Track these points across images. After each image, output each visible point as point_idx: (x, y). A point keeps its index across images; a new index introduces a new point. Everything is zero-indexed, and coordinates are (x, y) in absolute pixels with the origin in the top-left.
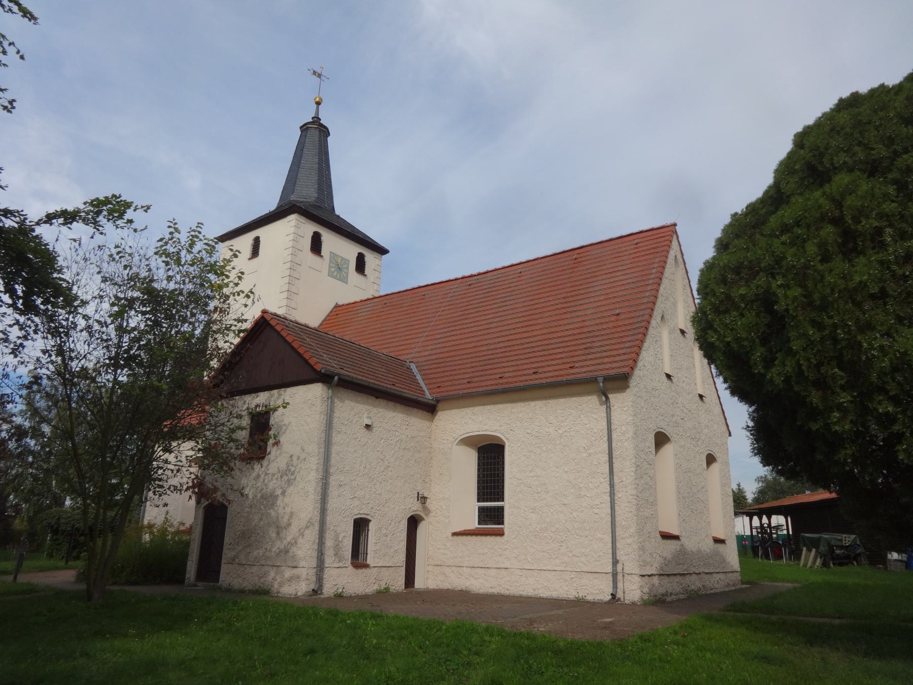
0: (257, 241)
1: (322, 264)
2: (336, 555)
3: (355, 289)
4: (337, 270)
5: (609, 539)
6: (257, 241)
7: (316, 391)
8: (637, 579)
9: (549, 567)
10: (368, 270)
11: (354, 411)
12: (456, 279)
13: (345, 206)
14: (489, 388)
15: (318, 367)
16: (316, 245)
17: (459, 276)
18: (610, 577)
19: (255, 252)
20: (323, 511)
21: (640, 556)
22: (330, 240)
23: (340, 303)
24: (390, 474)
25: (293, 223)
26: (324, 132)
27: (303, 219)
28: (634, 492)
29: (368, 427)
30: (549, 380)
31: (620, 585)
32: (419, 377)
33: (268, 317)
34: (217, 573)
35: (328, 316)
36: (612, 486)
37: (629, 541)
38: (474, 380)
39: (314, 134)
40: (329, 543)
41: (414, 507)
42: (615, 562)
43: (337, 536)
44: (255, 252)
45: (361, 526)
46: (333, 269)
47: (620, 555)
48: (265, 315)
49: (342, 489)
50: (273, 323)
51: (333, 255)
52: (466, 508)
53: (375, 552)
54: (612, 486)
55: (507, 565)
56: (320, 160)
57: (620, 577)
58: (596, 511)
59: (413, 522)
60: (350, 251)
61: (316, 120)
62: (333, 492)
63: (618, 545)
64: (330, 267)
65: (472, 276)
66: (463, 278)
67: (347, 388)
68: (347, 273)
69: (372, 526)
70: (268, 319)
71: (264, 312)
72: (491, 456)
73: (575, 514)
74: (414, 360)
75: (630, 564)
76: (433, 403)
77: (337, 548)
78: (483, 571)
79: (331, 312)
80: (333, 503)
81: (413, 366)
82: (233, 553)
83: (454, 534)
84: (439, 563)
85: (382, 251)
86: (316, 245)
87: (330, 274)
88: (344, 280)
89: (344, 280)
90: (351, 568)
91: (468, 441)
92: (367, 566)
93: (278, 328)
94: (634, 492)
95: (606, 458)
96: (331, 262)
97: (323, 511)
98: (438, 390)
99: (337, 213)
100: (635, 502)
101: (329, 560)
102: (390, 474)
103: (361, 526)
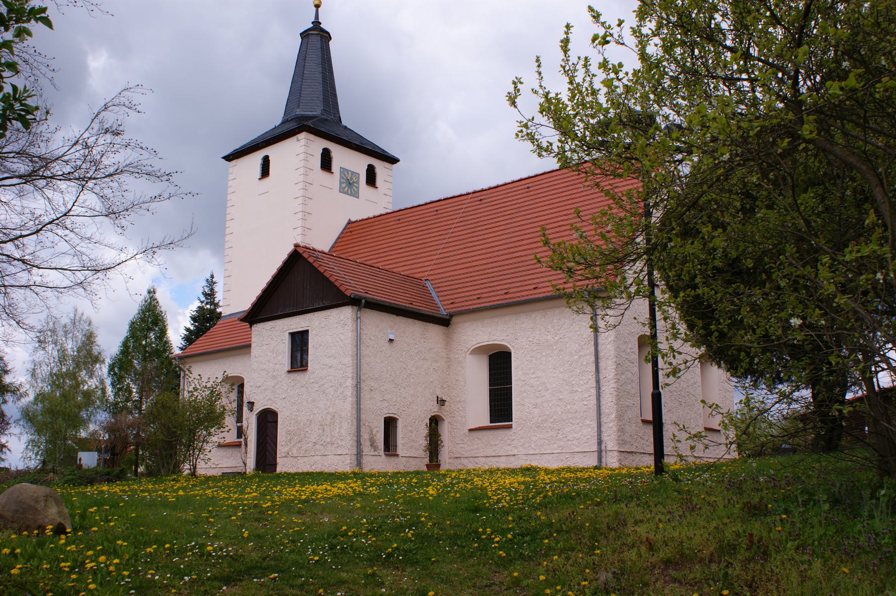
0: (266, 162)
1: (333, 180)
2: (372, 445)
3: (371, 204)
4: (349, 185)
5: (594, 425)
6: (266, 162)
7: (346, 313)
8: (616, 454)
9: (548, 451)
10: (379, 181)
11: (379, 326)
12: (468, 194)
13: (351, 116)
14: (495, 303)
15: (348, 293)
16: (326, 163)
17: (471, 191)
18: (596, 454)
19: (265, 171)
20: (359, 410)
21: (619, 436)
22: (342, 157)
23: (353, 220)
24: (412, 381)
25: (303, 142)
26: (325, 37)
27: (312, 137)
28: (614, 385)
29: (391, 340)
30: (544, 295)
31: (604, 460)
32: (434, 294)
33: (300, 250)
34: (275, 465)
35: (342, 233)
36: (598, 381)
37: (610, 425)
38: (483, 296)
39: (315, 41)
40: (365, 436)
41: (434, 410)
42: (600, 443)
43: (371, 431)
44: (265, 171)
45: (390, 424)
46: (344, 185)
47: (605, 438)
48: (298, 249)
49: (373, 393)
50: (305, 255)
51: (343, 171)
52: (478, 408)
53: (403, 445)
54: (598, 381)
55: (515, 452)
56: (324, 68)
57: (604, 454)
58: (585, 403)
59: (435, 422)
60: (358, 163)
61: (317, 23)
62: (365, 395)
63: (603, 429)
64: (341, 183)
65: (482, 190)
66: (474, 192)
67: (372, 309)
68: (358, 188)
69: (400, 424)
70: (301, 252)
71: (297, 246)
72: (500, 364)
73: (569, 407)
74: (429, 278)
75: (611, 443)
76: (447, 317)
77: (373, 444)
78: (496, 459)
79: (344, 229)
80: (366, 404)
81: (428, 284)
82: (286, 449)
83: (471, 430)
84: (458, 455)
85: (393, 160)
86: (326, 163)
87: (342, 190)
88: (356, 195)
89: (356, 195)
90: (384, 456)
91: (479, 351)
92: (397, 455)
93: (311, 260)
94: (614, 385)
95: (593, 359)
96: (341, 178)
97: (359, 410)
98: (478, 301)
99: (344, 123)
100: (615, 393)
101: (367, 449)
102: (412, 381)
103: (390, 424)
